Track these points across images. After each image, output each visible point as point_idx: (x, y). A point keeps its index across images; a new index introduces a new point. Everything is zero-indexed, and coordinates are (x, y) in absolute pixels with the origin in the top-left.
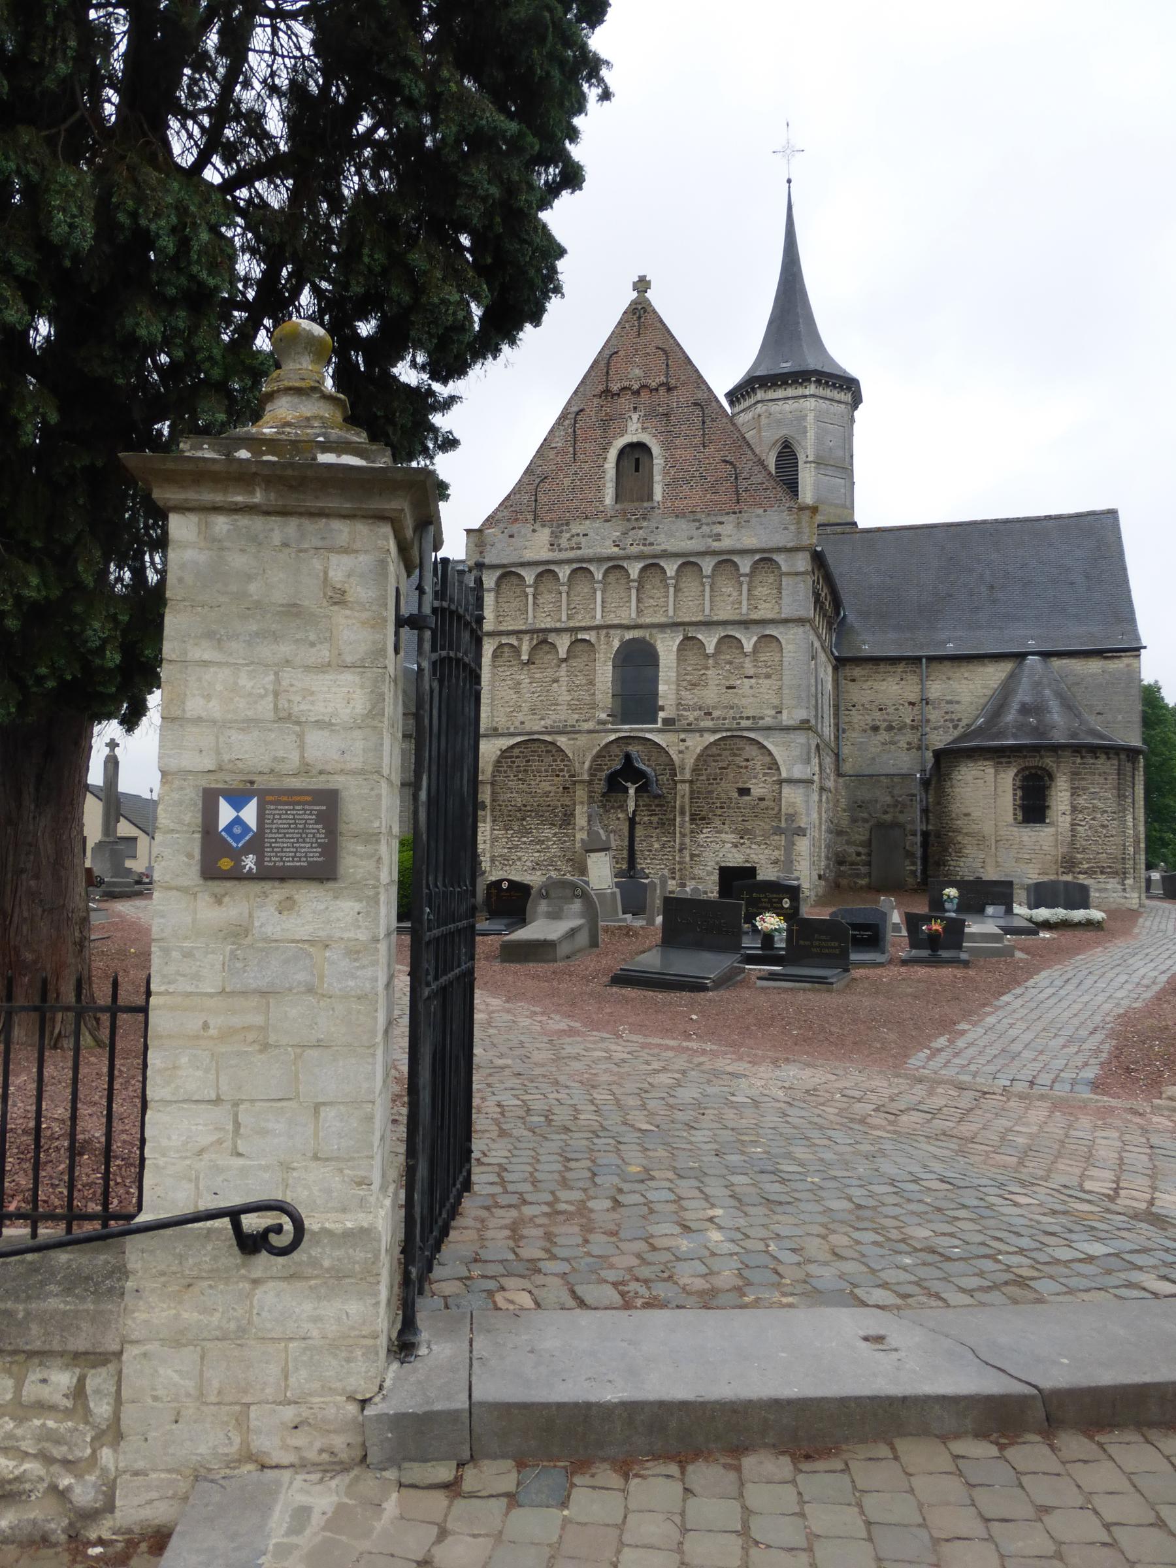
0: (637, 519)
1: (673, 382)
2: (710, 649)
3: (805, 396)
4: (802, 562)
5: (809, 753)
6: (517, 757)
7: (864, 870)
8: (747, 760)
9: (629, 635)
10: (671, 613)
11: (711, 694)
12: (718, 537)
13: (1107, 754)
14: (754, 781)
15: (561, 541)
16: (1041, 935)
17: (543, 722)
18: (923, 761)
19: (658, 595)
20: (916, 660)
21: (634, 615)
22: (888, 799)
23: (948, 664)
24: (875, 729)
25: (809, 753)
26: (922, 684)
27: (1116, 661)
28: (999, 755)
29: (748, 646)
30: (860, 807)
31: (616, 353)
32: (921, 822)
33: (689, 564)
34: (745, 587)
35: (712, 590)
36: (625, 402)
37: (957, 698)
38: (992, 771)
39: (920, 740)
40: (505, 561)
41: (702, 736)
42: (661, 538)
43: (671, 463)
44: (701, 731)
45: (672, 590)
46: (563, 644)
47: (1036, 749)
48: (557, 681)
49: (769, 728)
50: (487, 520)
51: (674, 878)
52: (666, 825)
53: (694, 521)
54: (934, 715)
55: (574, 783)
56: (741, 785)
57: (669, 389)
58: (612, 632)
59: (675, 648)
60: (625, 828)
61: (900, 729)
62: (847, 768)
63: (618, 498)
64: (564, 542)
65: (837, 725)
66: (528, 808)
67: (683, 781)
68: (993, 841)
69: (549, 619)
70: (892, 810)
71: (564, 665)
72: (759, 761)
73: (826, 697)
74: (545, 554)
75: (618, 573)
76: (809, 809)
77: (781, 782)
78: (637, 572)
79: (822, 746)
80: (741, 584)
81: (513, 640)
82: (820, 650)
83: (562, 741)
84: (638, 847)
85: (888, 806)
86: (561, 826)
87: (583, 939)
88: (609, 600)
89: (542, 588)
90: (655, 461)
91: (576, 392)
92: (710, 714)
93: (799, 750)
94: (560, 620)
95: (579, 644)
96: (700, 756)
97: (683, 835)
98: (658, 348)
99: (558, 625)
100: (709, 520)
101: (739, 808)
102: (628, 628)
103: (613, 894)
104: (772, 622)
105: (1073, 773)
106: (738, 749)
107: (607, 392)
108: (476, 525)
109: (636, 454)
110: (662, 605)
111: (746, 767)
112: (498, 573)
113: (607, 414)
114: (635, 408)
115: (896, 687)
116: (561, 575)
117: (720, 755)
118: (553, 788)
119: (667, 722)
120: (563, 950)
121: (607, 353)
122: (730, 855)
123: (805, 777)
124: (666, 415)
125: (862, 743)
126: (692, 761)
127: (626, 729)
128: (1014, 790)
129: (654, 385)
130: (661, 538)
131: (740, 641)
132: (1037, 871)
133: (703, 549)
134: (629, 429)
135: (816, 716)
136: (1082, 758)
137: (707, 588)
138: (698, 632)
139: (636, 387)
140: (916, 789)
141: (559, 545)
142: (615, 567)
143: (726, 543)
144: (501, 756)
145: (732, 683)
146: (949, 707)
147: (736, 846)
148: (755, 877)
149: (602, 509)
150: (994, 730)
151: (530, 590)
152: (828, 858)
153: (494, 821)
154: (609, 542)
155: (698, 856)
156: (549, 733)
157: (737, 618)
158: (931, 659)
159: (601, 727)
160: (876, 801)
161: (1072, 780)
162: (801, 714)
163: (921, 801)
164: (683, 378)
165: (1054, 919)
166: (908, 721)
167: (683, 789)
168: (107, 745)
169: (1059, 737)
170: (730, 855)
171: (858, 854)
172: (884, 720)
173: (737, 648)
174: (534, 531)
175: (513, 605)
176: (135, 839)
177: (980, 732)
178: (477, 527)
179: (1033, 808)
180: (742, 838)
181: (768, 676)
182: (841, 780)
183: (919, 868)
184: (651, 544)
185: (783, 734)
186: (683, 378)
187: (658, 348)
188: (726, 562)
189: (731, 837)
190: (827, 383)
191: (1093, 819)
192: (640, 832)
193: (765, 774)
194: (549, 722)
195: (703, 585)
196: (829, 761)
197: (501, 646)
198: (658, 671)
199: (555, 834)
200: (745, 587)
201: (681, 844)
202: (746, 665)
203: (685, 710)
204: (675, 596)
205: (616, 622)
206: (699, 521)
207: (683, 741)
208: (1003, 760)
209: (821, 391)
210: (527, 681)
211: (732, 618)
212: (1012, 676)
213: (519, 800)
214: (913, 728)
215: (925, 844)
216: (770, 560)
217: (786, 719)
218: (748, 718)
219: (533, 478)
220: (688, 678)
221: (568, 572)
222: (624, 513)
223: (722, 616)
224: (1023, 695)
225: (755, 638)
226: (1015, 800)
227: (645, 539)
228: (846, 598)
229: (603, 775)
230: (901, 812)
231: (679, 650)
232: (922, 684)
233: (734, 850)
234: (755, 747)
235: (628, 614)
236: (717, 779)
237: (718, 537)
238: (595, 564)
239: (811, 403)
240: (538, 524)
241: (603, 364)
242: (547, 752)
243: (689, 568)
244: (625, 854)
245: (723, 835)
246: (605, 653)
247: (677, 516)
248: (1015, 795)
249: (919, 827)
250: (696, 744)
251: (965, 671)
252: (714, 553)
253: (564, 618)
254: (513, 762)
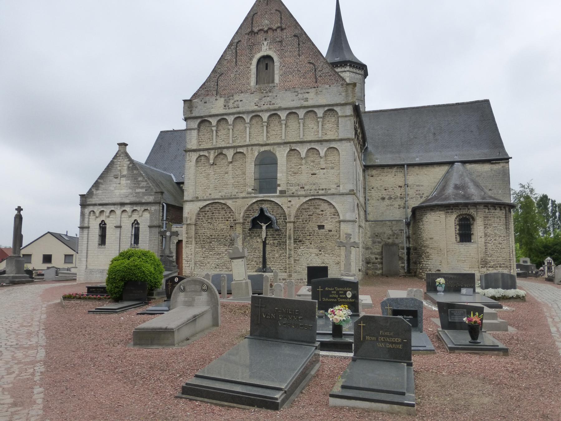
0: (266, 92)
1: (284, 26)
2: (303, 155)
3: (345, 71)
4: (349, 111)
5: (354, 207)
6: (208, 211)
7: (379, 266)
8: (323, 211)
9: (263, 149)
10: (283, 138)
11: (304, 178)
12: (306, 100)
13: (500, 207)
15: (229, 104)
16: (505, 308)
17: (220, 194)
18: (406, 214)
19: (277, 129)
20: (402, 166)
21: (265, 139)
22: (390, 232)
23: (417, 168)
24: (383, 199)
25: (354, 207)
26: (405, 177)
27: (497, 165)
28: (447, 208)
29: (322, 153)
30: (377, 236)
31: (256, 13)
32: (406, 243)
33: (292, 113)
34: (320, 124)
35: (304, 126)
36: (261, 36)
37: (422, 184)
38: (444, 216)
39: (405, 204)
40: (202, 115)
41: (299, 199)
43: (283, 65)
44: (299, 196)
45: (284, 126)
46: (230, 154)
47: (466, 205)
49: (333, 194)
50: (194, 95)
51: (286, 272)
52: (282, 244)
53: (295, 92)
54: (411, 192)
55: (236, 224)
56: (319, 224)
57: (282, 30)
58: (254, 148)
59: (285, 155)
60: (261, 246)
61: (395, 199)
62: (370, 217)
63: (257, 83)
64: (231, 104)
65: (365, 197)
66: (213, 237)
67: (290, 222)
68: (445, 252)
69: (223, 143)
70: (392, 237)
71: (231, 165)
72: (329, 211)
73: (360, 182)
74: (222, 111)
75: (257, 119)
76: (356, 233)
77: (340, 222)
78: (266, 117)
79: (359, 205)
80: (318, 122)
81: (205, 153)
82: (357, 157)
83: (229, 203)
84: (267, 256)
85: (390, 235)
86: (229, 246)
87: (206, 321)
88: (253, 132)
89: (220, 128)
90: (275, 64)
91: (237, 33)
92: (303, 188)
94: (229, 143)
95: (238, 155)
96: (299, 209)
97: (290, 250)
98: (276, 10)
99: (228, 145)
100: (302, 92)
101: (318, 235)
102: (262, 145)
103: (247, 283)
104: (334, 140)
105: (485, 217)
106: (318, 205)
107: (252, 32)
108: (188, 98)
109: (266, 61)
110: (279, 133)
111: (322, 215)
112: (199, 120)
113: (252, 43)
114: (266, 39)
116: (229, 121)
117: (309, 209)
118: (225, 227)
119: (282, 192)
120: (178, 337)
121: (252, 13)
122: (314, 260)
123: (352, 219)
124: (281, 42)
125: (377, 205)
126: (295, 212)
127: (261, 196)
128: (455, 226)
129: (275, 28)
131: (318, 151)
132: (469, 266)
133: (299, 106)
134: (263, 49)
135: (357, 190)
136: (489, 209)
137: (301, 125)
139: (266, 29)
140: (404, 227)
141: (228, 106)
142: (256, 116)
143: (310, 103)
144: (200, 211)
145: (314, 172)
146: (418, 188)
147: (317, 255)
148: (326, 274)
149: (249, 88)
150: (443, 197)
151: (214, 129)
152: (363, 261)
153: (196, 244)
155: (298, 260)
156: (223, 199)
157: (317, 139)
158: (409, 165)
159: (249, 195)
160: (384, 233)
161: (484, 220)
162: (350, 187)
163: (406, 233)
165: (497, 295)
167: (290, 226)
168: (16, 209)
169: (477, 199)
170: (314, 260)
171: (376, 259)
172: (387, 195)
173: (317, 154)
174: (216, 100)
176: (72, 255)
177: (435, 198)
178: (189, 99)
179: (465, 234)
180: (320, 251)
181: (332, 168)
182: (367, 223)
183: (406, 265)
184: (274, 104)
185: (341, 197)
187: (276, 10)
188: (311, 111)
189: (316, 251)
190: (354, 66)
191: (495, 240)
192: (268, 248)
193: (332, 218)
195: (299, 123)
196: (362, 213)
197: (200, 156)
198: (277, 167)
200: (320, 124)
201: (289, 254)
202: (321, 163)
203: (291, 186)
204: (286, 130)
205: (256, 143)
206: (297, 92)
207: (290, 201)
208: (450, 211)
209: (351, 69)
210: (213, 173)
211: (313, 139)
212: (448, 172)
213: (208, 233)
214: (401, 198)
215: (408, 254)
216: (333, 110)
217: (342, 189)
218: (323, 189)
219: (216, 74)
220: (292, 170)
221: (233, 119)
222: (260, 89)
223: (309, 139)
224: (455, 180)
225: (326, 149)
226: (456, 231)
227: (270, 102)
228: (369, 140)
229: (250, 220)
230: (397, 238)
231: (287, 156)
232: (405, 177)
233: (316, 257)
234: (326, 204)
235: (262, 139)
236: (306, 221)
237: (306, 100)
238: (246, 115)
239: (348, 74)
240: (218, 96)
241: (250, 19)
242: (222, 208)
243: (292, 116)
244: (261, 260)
248: (456, 228)
249: (405, 245)
250: (297, 203)
251: (425, 170)
252: (305, 107)
253: (231, 142)
254: (206, 214)
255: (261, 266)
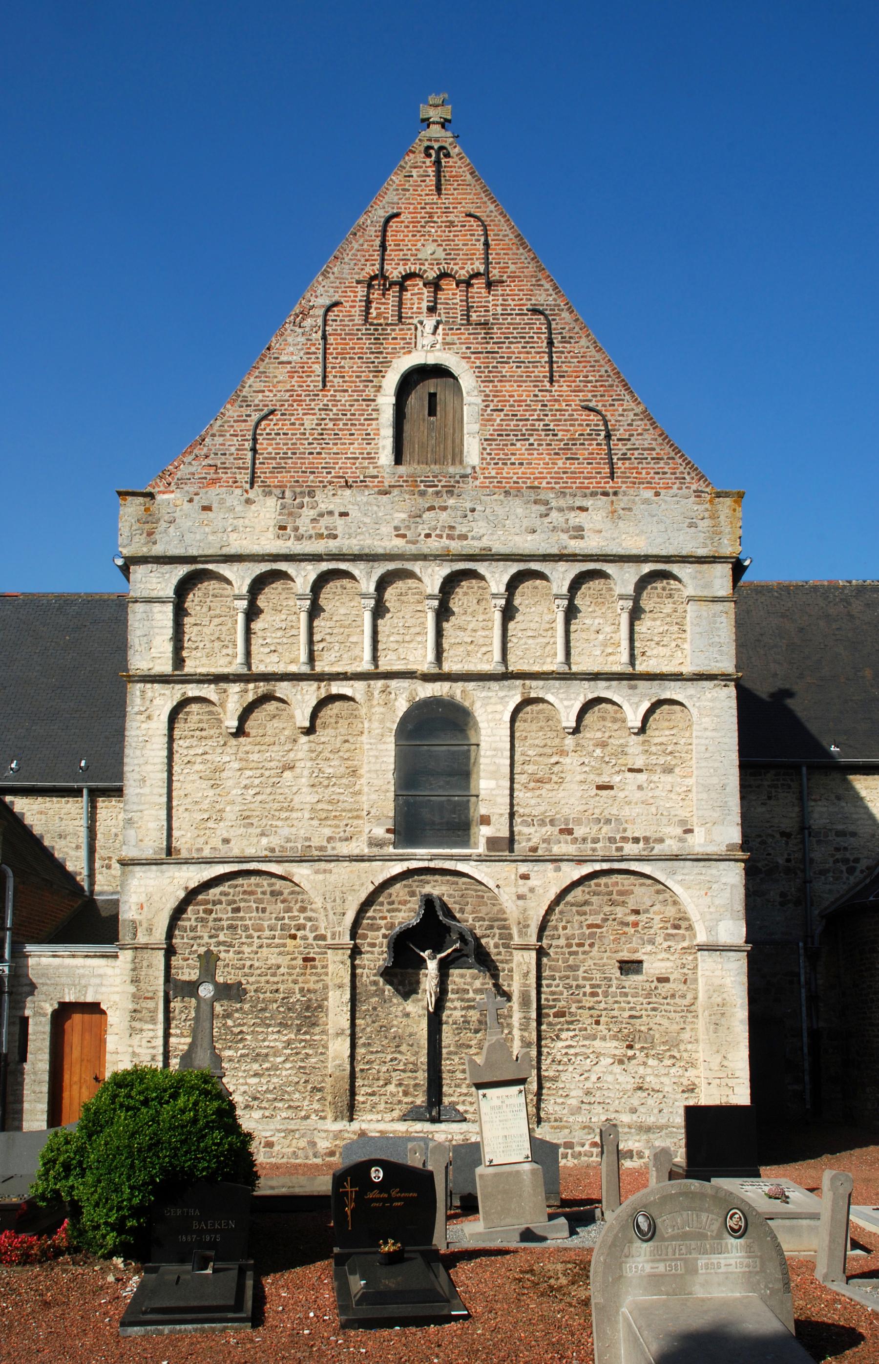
8: (637, 912)
11: (571, 797)
14: (649, 948)
15: (299, 522)
17: (264, 841)
31: (397, 215)
37: (851, 828)
40: (193, 552)
42: (480, 527)
43: (492, 405)
44: (556, 860)
48: (292, 768)
49: (676, 858)
56: (626, 955)
57: (489, 285)
69: (274, 658)
74: (271, 544)
81: (208, 691)
83: (301, 873)
92: (570, 832)
93: (727, 894)
98: (470, 215)
100: (562, 503)
104: (677, 677)
109: (424, 383)
111: (635, 924)
112: (182, 570)
115: (761, 809)
127: (422, 855)
130: (480, 527)
133: (555, 551)
138: (548, 690)
141: (296, 529)
143: (591, 544)
145: (604, 779)
154: (387, 529)
159: (376, 851)
164: (512, 267)
166: (781, 861)
170: (610, 1078)
174: (248, 501)
175: (206, 630)
181: (668, 770)
184: (463, 537)
186: (512, 267)
194: (275, 841)
199: (288, 1043)
202: (630, 750)
206: (547, 503)
207: (525, 877)
210: (236, 765)
217: (698, 843)
218: (636, 840)
227: (452, 528)
233: (617, 1069)
237: (578, 532)
245: (597, 1043)
246: (382, 721)
247: (507, 493)
250: (549, 881)
255: (420, 1100)
